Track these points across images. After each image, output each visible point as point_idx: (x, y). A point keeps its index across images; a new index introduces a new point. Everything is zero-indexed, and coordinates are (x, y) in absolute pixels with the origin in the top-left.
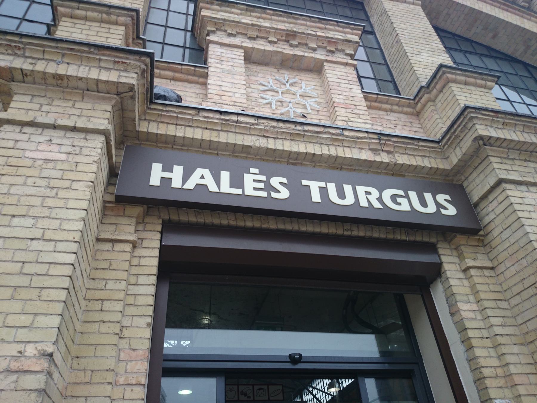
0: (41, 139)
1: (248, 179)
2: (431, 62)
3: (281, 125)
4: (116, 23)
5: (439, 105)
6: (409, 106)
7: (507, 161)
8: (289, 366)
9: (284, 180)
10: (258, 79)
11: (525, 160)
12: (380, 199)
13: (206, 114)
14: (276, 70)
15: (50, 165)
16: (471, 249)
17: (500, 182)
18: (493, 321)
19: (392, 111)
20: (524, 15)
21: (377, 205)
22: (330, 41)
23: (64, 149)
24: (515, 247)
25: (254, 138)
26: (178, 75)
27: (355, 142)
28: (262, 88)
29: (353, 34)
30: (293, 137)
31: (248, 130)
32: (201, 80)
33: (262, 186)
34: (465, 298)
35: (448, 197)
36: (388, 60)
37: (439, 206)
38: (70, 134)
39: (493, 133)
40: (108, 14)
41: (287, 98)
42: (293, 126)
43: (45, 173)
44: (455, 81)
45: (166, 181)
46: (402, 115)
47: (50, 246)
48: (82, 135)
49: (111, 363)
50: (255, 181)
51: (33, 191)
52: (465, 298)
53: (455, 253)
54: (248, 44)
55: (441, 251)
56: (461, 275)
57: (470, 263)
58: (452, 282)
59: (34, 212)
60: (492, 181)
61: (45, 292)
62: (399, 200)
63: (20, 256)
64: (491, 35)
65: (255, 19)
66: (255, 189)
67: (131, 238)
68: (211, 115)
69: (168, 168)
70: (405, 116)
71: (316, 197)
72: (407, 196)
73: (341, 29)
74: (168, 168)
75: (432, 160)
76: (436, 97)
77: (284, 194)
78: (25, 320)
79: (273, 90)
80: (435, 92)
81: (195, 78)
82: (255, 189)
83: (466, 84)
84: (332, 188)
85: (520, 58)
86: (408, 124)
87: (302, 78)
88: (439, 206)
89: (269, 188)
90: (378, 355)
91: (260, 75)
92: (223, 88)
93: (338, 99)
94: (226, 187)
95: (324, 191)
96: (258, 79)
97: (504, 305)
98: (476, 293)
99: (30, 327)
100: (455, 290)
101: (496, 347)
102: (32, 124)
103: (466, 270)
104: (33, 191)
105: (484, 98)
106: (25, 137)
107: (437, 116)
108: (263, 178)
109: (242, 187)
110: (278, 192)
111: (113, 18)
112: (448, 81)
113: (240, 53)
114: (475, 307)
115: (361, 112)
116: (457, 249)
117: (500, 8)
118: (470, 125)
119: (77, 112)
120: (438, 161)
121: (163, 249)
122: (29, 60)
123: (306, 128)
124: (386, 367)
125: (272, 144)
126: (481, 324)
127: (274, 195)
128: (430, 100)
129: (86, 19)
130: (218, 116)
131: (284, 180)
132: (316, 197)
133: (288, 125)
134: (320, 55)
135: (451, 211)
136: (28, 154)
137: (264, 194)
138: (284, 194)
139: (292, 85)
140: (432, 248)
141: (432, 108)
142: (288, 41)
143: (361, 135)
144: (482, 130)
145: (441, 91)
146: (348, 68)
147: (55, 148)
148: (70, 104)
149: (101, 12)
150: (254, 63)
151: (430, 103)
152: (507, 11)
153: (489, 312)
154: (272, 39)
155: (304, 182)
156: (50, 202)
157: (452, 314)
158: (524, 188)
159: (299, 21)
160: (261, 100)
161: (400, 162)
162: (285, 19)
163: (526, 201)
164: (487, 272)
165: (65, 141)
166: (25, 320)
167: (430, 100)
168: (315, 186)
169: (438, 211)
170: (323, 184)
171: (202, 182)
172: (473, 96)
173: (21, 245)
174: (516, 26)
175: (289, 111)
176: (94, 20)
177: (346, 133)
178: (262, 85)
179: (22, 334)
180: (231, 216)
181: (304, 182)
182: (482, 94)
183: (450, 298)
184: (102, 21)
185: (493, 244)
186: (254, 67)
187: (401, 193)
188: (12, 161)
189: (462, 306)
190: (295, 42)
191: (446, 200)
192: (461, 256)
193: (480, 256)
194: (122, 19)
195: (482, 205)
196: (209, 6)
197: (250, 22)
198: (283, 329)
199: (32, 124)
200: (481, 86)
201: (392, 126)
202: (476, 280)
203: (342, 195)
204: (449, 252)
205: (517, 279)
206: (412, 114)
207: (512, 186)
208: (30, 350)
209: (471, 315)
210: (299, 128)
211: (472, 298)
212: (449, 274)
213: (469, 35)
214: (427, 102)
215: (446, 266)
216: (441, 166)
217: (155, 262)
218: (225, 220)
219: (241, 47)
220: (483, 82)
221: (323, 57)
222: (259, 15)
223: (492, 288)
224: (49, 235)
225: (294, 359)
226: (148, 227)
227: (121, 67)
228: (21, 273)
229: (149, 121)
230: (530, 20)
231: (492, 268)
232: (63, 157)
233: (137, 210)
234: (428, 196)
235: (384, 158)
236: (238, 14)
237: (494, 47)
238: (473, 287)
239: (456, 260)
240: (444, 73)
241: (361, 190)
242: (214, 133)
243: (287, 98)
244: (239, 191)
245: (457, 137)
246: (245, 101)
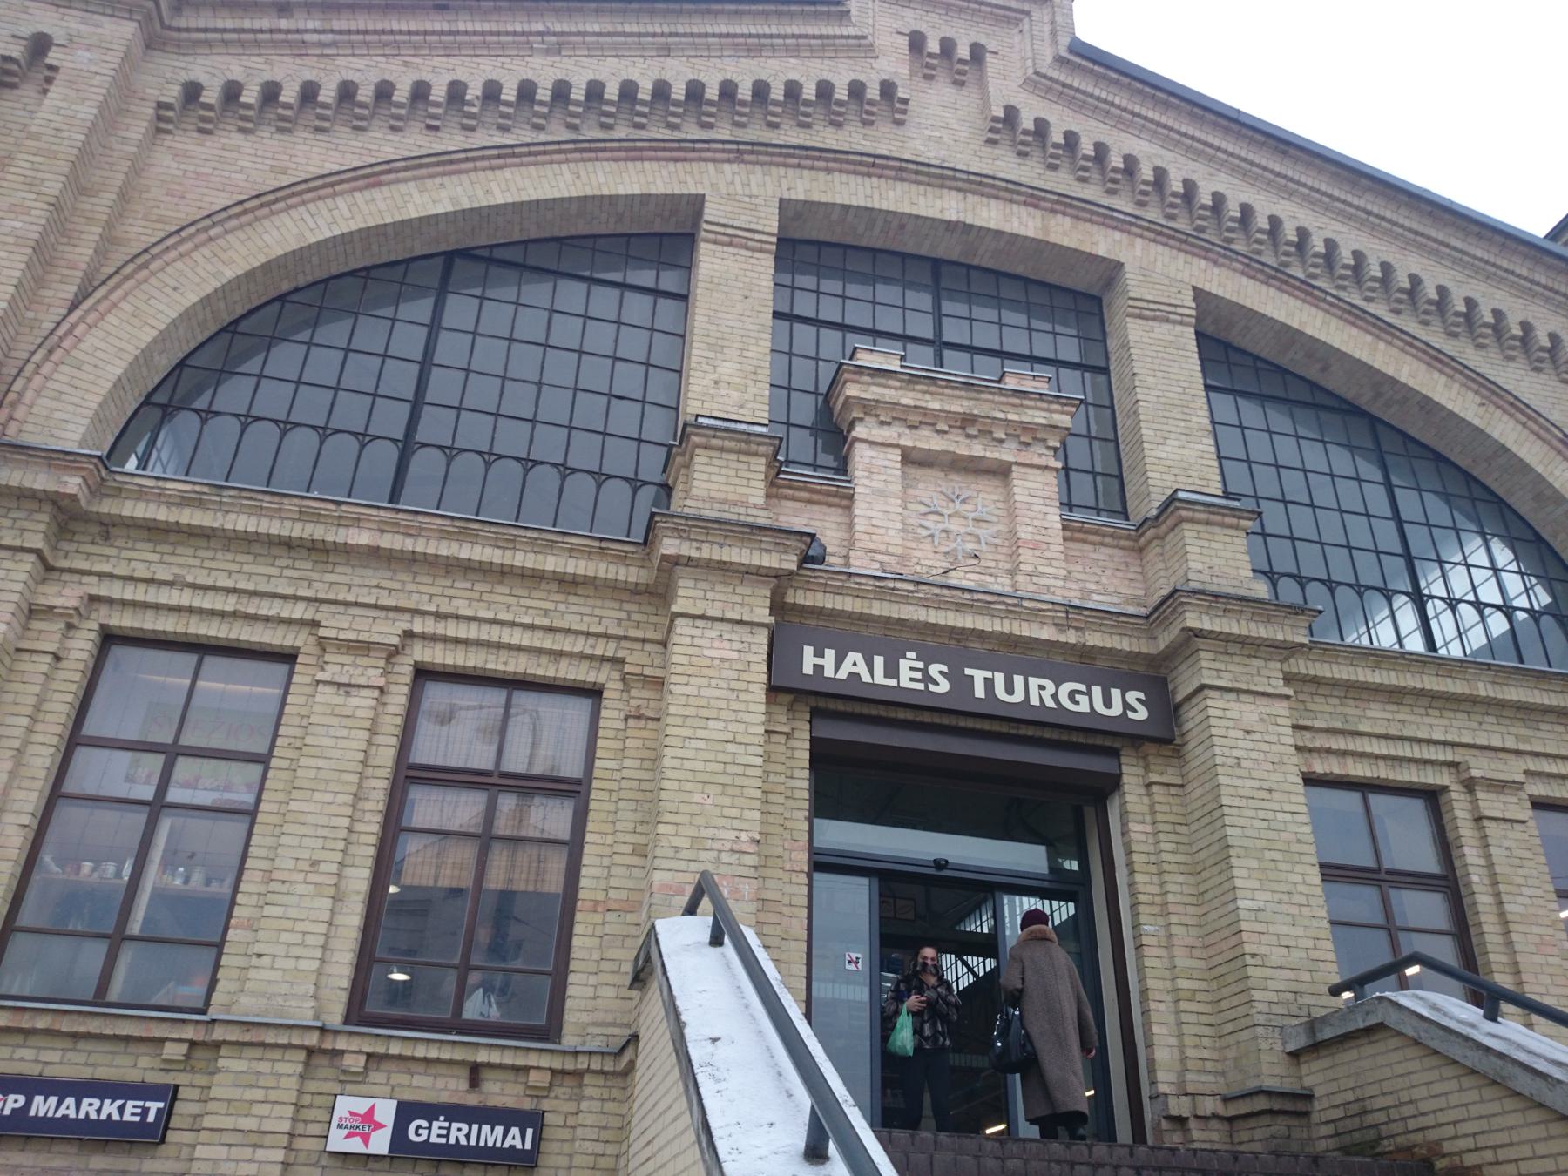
0: (714, 634)
1: (904, 665)
2: (1178, 457)
3: (945, 592)
4: (756, 454)
5: (1167, 547)
6: (1129, 538)
7: (1222, 657)
8: (932, 871)
9: (945, 668)
10: (917, 492)
11: (1249, 656)
12: (1055, 697)
13: (858, 580)
14: (942, 475)
15: (727, 665)
16: (1161, 760)
17: (1202, 687)
18: (1163, 846)
19: (1102, 544)
20: (1383, 335)
21: (1050, 703)
22: (1026, 427)
23: (737, 646)
24: (1203, 768)
25: (912, 608)
26: (816, 497)
27: (1036, 616)
28: (923, 509)
29: (1062, 413)
30: (959, 607)
31: (906, 598)
32: (845, 502)
33: (918, 675)
34: (1140, 818)
35: (1141, 695)
36: (1119, 433)
37: (1127, 706)
38: (737, 628)
39: (1206, 624)
40: (747, 442)
41: (955, 526)
42: (959, 593)
43: (725, 674)
44: (1192, 521)
45: (819, 668)
46: (1116, 551)
47: (741, 749)
48: (748, 629)
49: (779, 851)
50: (912, 669)
51: (717, 693)
52: (1140, 818)
53: (1141, 763)
54: (906, 442)
55: (1123, 760)
56: (1142, 791)
57: (1154, 777)
58: (1129, 798)
59: (723, 715)
60: (1195, 685)
61: (746, 791)
62: (1078, 697)
63: (721, 757)
64: (1318, 366)
65: (919, 396)
66: (912, 679)
67: (786, 729)
68: (863, 580)
69: (819, 653)
70: (1121, 553)
71: (980, 692)
72: (1089, 693)
73: (1045, 405)
74: (819, 653)
75: (1134, 640)
76: (1166, 534)
77: (944, 686)
78: (735, 812)
79: (937, 513)
80: (1164, 528)
81: (836, 500)
82: (912, 679)
83: (1208, 523)
84: (999, 679)
85: (1366, 408)
86: (1123, 567)
87: (980, 487)
88: (1127, 706)
89: (927, 679)
90: (1046, 871)
91: (921, 486)
92: (874, 522)
93: (1025, 533)
94: (880, 678)
95: (989, 683)
96: (917, 492)
97: (1183, 829)
98: (1153, 813)
99: (740, 818)
100: (1130, 807)
101: (1160, 874)
102: (702, 617)
103: (1149, 785)
104: (717, 693)
105: (1229, 547)
106: (697, 632)
107: (1161, 565)
108: (920, 665)
109: (897, 678)
110: (937, 683)
111: (753, 447)
112: (1182, 520)
113: (896, 455)
114: (1149, 829)
115: (1054, 555)
116: (1145, 758)
117: (1341, 318)
118: (1180, 610)
119: (738, 599)
120: (1143, 641)
121: (812, 740)
122: (695, 544)
123: (977, 596)
124: (1054, 886)
125: (933, 617)
126: (1151, 849)
127: (932, 688)
128: (1157, 537)
129: (722, 449)
130: (871, 582)
131: (945, 668)
132: (980, 692)
133: (954, 592)
134: (1006, 454)
135: (1142, 714)
136: (707, 652)
137: (921, 686)
138: (944, 686)
139: (964, 501)
140: (1115, 753)
141: (1158, 550)
142: (963, 428)
143: (1044, 606)
144: (1193, 620)
145: (1172, 529)
146: (1047, 473)
147: (726, 645)
148: (730, 589)
149: (739, 441)
150: (913, 463)
151: (1156, 542)
152: (1353, 324)
153: (1162, 837)
154: (942, 426)
155: (968, 671)
156: (734, 705)
157: (1123, 834)
158: (1232, 696)
159: (983, 396)
160: (920, 530)
161: (1091, 643)
162: (963, 393)
163: (1229, 714)
164: (1173, 791)
165: (734, 637)
166: (735, 812)
167: (1157, 537)
168: (979, 676)
169: (1124, 713)
170: (989, 674)
171: (855, 670)
172: (1214, 545)
173: (719, 747)
174: (1359, 361)
175: (955, 550)
176: (730, 451)
177: (1026, 604)
178: (923, 504)
179: (736, 824)
180: (881, 707)
181: (968, 671)
182: (1228, 539)
183: (1124, 814)
184: (739, 452)
185: (1188, 757)
186: (914, 472)
187: (1083, 688)
188: (695, 660)
189: (1133, 826)
190: (973, 431)
191: (1138, 700)
192: (1147, 768)
193: (1170, 770)
194: (762, 449)
195: (1185, 707)
196: (855, 377)
197: (912, 403)
198: (925, 829)
199: (702, 617)
200: (1230, 527)
201: (1098, 571)
202: (1157, 798)
203: (1010, 690)
204: (1134, 761)
205: (1199, 803)
206: (1133, 549)
207: (1216, 694)
208: (744, 836)
209: (1143, 837)
210: (967, 596)
211: (1148, 818)
212: (1126, 788)
213: (1284, 361)
214: (1150, 542)
215: (1125, 779)
216: (1144, 650)
217: (807, 755)
218: (874, 711)
219: (897, 446)
220: (1234, 521)
221: (1011, 458)
222: (925, 388)
223: (1175, 809)
224: (739, 738)
225: (939, 864)
226: (798, 715)
227: (781, 548)
228: (724, 773)
229: (796, 589)
230: (1390, 343)
231: (1182, 786)
232: (735, 655)
233: (787, 698)
234: (1116, 694)
235: (1071, 637)
236: (896, 388)
237: (1323, 383)
238: (1152, 806)
239: (1141, 771)
240: (1177, 508)
241: (1034, 682)
242: (866, 603)
243: (955, 526)
244: (893, 682)
245: (1167, 618)
246: (899, 541)
